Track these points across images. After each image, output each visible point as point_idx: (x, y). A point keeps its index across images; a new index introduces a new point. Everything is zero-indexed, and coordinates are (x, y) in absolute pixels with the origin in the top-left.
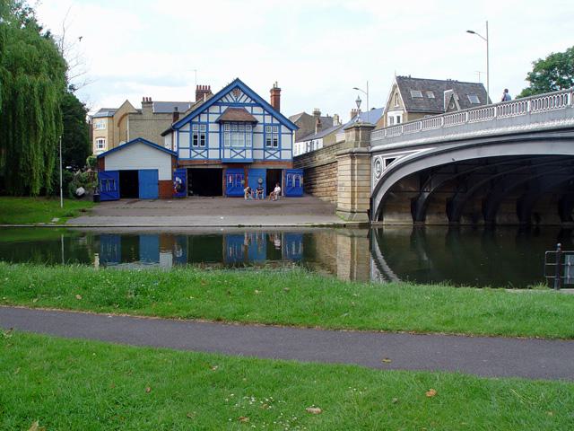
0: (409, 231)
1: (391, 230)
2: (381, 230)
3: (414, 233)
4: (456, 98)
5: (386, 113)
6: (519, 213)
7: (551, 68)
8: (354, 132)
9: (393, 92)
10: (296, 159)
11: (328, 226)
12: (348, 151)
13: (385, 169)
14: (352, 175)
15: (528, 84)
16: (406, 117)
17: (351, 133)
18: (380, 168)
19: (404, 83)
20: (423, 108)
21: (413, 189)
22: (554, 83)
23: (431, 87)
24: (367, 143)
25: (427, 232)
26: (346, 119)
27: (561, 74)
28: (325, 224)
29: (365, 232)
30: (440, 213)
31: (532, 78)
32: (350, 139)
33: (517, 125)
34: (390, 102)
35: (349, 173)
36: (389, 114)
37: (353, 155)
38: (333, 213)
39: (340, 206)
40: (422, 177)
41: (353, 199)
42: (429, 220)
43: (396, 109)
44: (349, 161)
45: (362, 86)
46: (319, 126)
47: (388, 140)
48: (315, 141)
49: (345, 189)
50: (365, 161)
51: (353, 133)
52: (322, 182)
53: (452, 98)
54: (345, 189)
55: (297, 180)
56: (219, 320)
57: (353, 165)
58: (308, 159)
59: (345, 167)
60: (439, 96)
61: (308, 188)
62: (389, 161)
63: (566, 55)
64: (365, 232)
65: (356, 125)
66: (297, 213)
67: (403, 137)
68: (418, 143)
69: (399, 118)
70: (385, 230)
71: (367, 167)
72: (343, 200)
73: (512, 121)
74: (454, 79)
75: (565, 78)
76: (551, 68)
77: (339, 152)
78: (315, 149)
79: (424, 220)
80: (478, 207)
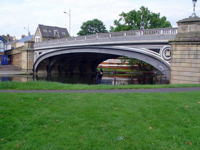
0: (46, 76)
1: (40, 76)
2: (37, 76)
3: (48, 76)
4: (58, 33)
5: (35, 37)
6: (80, 70)
7: (88, 25)
8: (28, 43)
9: (37, 30)
10: (5, 51)
11: (20, 74)
12: (26, 49)
13: (39, 56)
14: (27, 58)
15: (81, 30)
16: (42, 38)
17: (27, 44)
18: (37, 55)
19: (41, 27)
20: (47, 36)
21: (47, 62)
22: (89, 30)
23: (50, 29)
24: (32, 47)
25: (52, 76)
26: (19, 38)
27: (91, 27)
28: (19, 74)
29: (32, 76)
30: (56, 70)
31: (82, 28)
32: (26, 46)
33: (82, 43)
34: (36, 33)
35: (26, 57)
36: (36, 37)
37: (27, 51)
38: (20, 70)
39: (23, 68)
40: (50, 59)
41: (27, 65)
42: (52, 72)
43: (38, 36)
44: (26, 53)
45: (26, 27)
46: (9, 40)
47: (40, 46)
48: (8, 45)
49: (24, 62)
50: (32, 53)
51: (27, 44)
52: (15, 60)
53: (57, 33)
54: (24, 62)
55: (6, 59)
56: (38, 90)
57: (27, 54)
58: (9, 52)
59: (24, 55)
60: (53, 32)
61: (10, 62)
62: (40, 53)
63: (92, 21)
64: (32, 76)
65: (29, 41)
66: (8, 70)
67: (45, 46)
68: (51, 48)
69: (39, 38)
70: (39, 76)
71: (32, 55)
72: (24, 66)
73: (81, 42)
74: (57, 26)
75: (92, 28)
76: (88, 25)
77: (22, 50)
78: (8, 49)
79: (51, 72)
80: (68, 68)
